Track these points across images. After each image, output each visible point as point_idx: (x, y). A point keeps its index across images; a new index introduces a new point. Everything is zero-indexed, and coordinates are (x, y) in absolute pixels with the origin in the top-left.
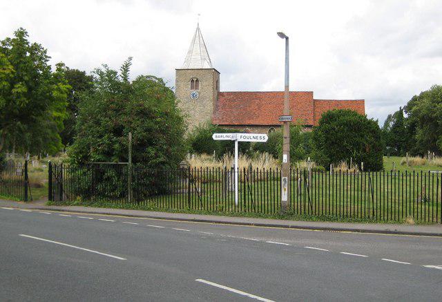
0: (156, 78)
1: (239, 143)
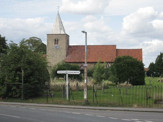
0: (37, 38)
1: (68, 74)
